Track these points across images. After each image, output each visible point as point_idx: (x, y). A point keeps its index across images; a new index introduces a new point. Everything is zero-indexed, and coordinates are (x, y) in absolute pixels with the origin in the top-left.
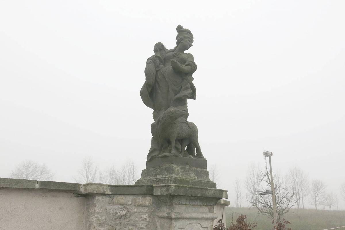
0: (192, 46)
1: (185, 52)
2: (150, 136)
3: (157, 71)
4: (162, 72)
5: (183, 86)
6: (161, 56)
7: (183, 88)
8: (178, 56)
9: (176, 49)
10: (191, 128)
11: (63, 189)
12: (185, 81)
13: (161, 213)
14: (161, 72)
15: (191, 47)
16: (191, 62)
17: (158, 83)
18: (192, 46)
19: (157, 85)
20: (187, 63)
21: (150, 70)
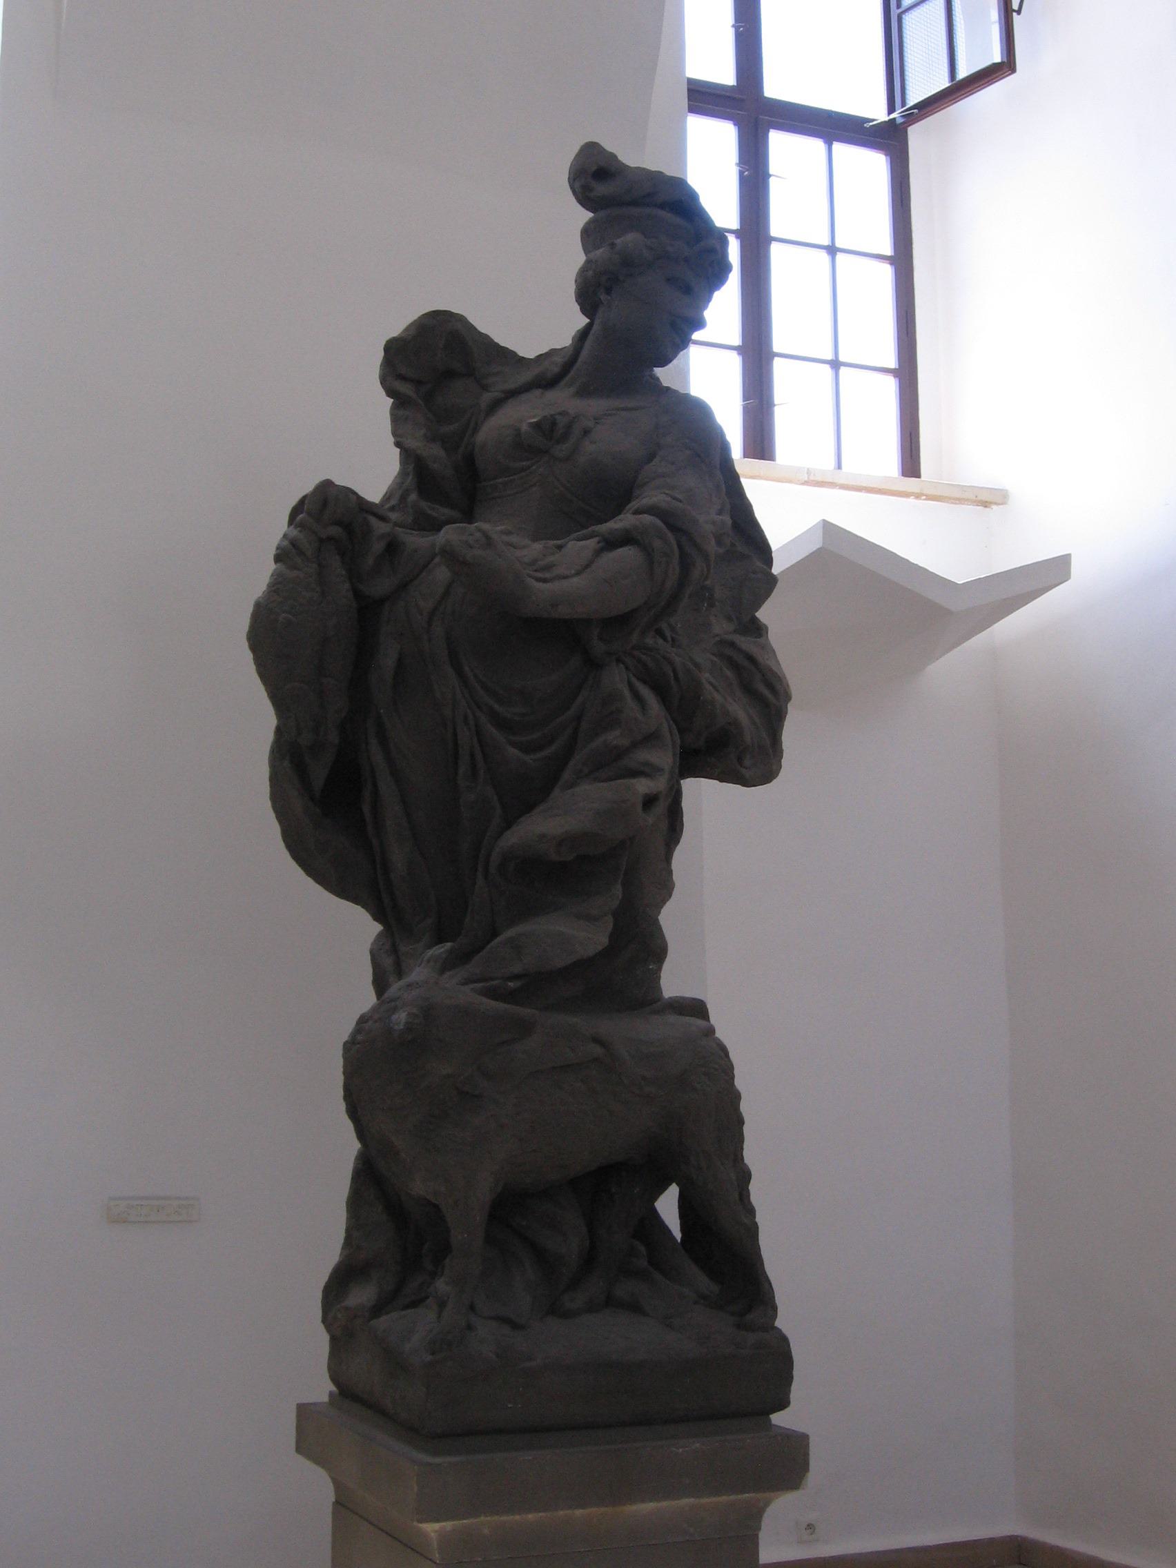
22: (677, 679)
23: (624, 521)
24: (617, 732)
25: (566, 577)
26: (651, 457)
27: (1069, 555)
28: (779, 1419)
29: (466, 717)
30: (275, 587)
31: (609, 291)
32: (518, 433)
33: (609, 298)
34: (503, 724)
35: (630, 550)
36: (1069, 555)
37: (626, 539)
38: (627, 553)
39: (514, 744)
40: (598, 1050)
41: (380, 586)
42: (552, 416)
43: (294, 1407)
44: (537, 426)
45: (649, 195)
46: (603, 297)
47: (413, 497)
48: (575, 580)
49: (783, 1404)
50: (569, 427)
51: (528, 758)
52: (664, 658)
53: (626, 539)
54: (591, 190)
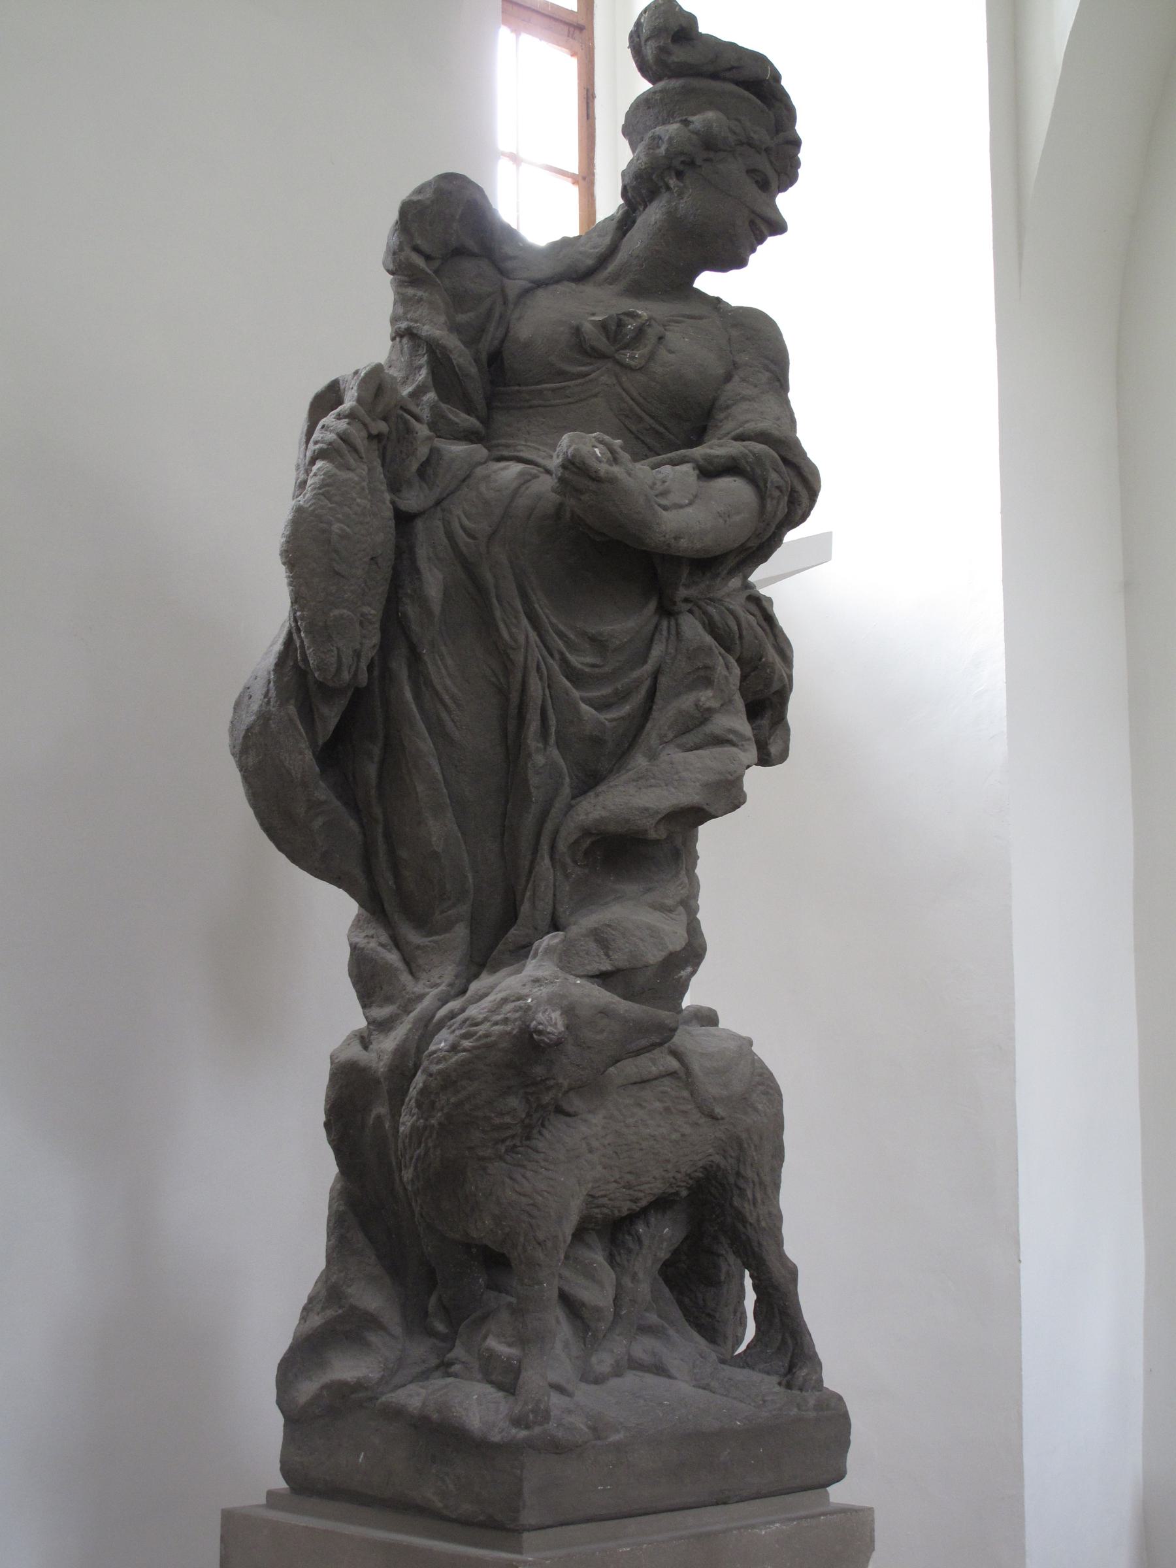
0: (778, 227)
1: (708, 282)
2: (986, 44)
3: (404, 520)
4: (462, 537)
5: (663, 681)
6: (410, 1166)
7: (663, 717)
8: (627, 356)
9: (613, 250)
10: (719, 1111)
11: (483, 1001)
12: (692, 628)
13: (403, 259)
14: (450, 536)
15: (772, 243)
16: (763, 437)
17: (415, 658)
18: (778, 227)
19: (400, 667)
20: (717, 448)
21: (344, 536)
22: (741, 636)
23: (717, 448)
24: (710, 693)
25: (681, 507)
26: (728, 378)
27: (831, 533)
28: (838, 1494)
29: (538, 668)
30: (324, 489)
31: (679, 175)
32: (577, 331)
33: (681, 185)
34: (576, 677)
35: (735, 481)
36: (831, 533)
37: (732, 468)
38: (733, 487)
39: (584, 700)
40: (674, 1064)
41: (412, 501)
42: (618, 315)
43: (219, 1513)
44: (603, 326)
45: (731, 68)
46: (672, 182)
47: (431, 396)
48: (690, 510)
49: (839, 1476)
50: (640, 332)
51: (604, 717)
52: (728, 609)
53: (732, 468)
54: (669, 53)
